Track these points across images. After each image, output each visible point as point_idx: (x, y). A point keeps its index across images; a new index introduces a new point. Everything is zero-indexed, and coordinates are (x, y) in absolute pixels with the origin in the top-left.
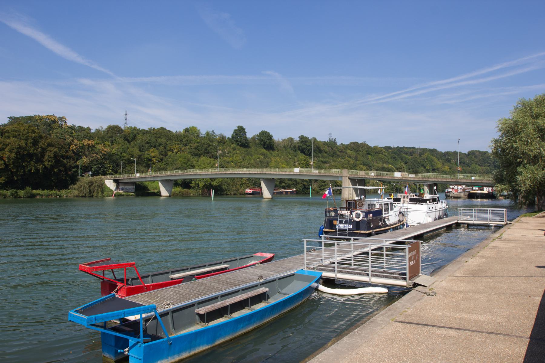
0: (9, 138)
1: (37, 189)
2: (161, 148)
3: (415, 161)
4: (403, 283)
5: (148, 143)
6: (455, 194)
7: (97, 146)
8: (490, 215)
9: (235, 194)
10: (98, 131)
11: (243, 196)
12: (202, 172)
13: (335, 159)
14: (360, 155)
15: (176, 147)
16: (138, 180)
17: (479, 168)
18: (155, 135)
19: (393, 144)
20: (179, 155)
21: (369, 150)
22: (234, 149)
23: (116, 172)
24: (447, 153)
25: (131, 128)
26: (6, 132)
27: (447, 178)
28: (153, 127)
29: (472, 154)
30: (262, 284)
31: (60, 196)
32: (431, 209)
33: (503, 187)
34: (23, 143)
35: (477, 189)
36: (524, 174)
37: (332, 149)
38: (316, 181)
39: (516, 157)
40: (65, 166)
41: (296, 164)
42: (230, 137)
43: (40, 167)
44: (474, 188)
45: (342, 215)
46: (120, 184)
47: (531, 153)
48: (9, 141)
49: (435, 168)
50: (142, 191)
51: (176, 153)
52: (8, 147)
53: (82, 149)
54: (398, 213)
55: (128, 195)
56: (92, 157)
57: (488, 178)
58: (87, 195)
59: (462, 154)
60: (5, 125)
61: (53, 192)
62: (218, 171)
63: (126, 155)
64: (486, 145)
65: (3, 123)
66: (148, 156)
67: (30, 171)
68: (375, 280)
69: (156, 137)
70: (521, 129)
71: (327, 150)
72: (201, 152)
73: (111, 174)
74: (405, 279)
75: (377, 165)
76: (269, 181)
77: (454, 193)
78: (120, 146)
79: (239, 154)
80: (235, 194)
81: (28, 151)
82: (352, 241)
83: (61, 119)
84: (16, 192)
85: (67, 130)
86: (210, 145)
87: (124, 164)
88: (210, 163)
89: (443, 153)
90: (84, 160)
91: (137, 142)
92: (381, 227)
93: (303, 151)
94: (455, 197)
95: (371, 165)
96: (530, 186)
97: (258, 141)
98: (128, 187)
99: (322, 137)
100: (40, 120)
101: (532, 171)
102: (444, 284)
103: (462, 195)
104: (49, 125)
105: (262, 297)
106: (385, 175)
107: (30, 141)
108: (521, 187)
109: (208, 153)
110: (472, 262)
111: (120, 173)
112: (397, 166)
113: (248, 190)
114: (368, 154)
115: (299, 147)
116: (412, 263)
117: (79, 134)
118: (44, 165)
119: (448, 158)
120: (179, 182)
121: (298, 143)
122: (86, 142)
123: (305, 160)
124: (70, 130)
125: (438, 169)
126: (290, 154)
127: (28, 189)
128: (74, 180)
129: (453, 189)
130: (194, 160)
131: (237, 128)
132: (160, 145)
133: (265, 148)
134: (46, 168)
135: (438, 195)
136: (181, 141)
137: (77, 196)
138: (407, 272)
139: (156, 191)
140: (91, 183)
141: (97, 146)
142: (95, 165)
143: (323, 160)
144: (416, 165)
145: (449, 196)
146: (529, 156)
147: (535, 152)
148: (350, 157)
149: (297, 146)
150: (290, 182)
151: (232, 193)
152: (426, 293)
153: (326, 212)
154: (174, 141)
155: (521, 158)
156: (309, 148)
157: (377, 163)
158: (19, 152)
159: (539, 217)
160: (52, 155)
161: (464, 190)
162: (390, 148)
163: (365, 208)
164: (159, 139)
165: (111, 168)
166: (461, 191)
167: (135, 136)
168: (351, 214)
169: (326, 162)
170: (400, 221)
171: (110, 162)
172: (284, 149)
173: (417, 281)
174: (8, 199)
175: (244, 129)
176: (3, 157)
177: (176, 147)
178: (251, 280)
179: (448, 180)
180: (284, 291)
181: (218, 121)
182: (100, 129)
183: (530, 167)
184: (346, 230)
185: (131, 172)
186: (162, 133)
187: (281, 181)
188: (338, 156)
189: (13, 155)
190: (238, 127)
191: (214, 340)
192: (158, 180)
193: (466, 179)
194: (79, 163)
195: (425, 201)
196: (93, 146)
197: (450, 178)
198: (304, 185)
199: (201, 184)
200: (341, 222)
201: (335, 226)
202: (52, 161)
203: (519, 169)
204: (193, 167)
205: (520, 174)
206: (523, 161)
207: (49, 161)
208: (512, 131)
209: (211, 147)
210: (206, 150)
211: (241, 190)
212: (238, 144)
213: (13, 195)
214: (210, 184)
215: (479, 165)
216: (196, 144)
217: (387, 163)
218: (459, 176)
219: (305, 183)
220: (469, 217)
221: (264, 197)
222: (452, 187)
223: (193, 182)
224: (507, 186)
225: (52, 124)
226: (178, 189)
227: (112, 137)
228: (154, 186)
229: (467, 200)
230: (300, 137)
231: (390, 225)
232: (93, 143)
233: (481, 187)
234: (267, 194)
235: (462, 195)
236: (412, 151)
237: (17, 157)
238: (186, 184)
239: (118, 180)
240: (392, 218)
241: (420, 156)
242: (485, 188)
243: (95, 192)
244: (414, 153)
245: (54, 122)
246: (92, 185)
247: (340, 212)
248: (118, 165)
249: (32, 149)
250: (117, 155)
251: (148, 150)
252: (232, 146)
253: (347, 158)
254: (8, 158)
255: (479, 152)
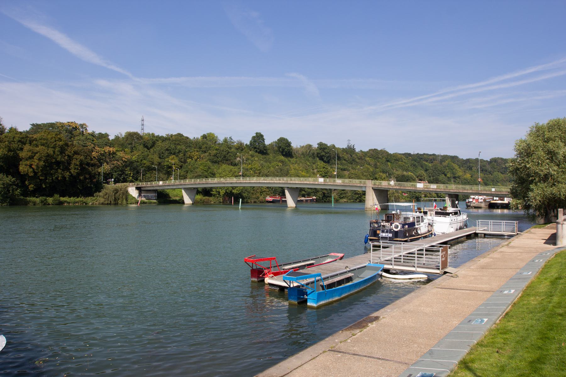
0: (37, 146)
1: (64, 197)
2: (181, 155)
3: (435, 168)
4: (438, 271)
5: (167, 150)
6: (476, 204)
7: (118, 153)
8: (503, 227)
9: (255, 202)
10: (117, 138)
11: (263, 204)
12: (222, 181)
13: (354, 166)
14: (379, 162)
15: (195, 154)
16: (161, 188)
17: (501, 176)
18: (174, 142)
19: (413, 151)
20: (200, 162)
21: (389, 157)
22: (252, 156)
23: (137, 180)
24: (468, 161)
25: (149, 134)
26: (34, 140)
27: (468, 189)
28: (171, 133)
29: (494, 161)
30: (349, 271)
31: (86, 204)
32: (453, 221)
33: (518, 201)
34: (51, 151)
35: (497, 198)
36: (536, 191)
37: (351, 156)
38: (335, 190)
39: (529, 175)
40: (90, 173)
41: (315, 171)
42: (248, 143)
43: (67, 174)
44: (495, 198)
45: (384, 226)
46: (142, 192)
47: (542, 173)
48: (38, 149)
49: (456, 175)
50: (163, 198)
51: (196, 160)
52: (37, 155)
53: (103, 156)
54: (427, 225)
55: (151, 203)
56: (113, 164)
57: (505, 189)
58: (112, 202)
59: (484, 161)
60: (27, 132)
61: (79, 199)
62: (241, 180)
63: (147, 163)
64: (508, 153)
65: (25, 130)
66: (168, 163)
67: (57, 178)
68: (419, 270)
69: (175, 144)
70: (533, 151)
71: (346, 157)
72: (220, 159)
73: (131, 181)
74: (439, 269)
75: (397, 173)
76: (293, 190)
77: (474, 204)
78: (140, 153)
79: (258, 161)
80: (255, 202)
81: (56, 159)
82: (402, 245)
83: (82, 126)
84: (46, 200)
85: (88, 137)
86: (229, 152)
87: (144, 171)
88: (231, 171)
89: (464, 160)
90: (105, 168)
91: (157, 149)
92: (414, 236)
93: (321, 158)
94: (475, 207)
95: (390, 172)
96: (540, 201)
97: (276, 148)
98: (150, 195)
99: (341, 144)
100: (62, 127)
101: (542, 188)
102: (463, 272)
103: (483, 205)
104: (71, 132)
105: (349, 279)
106: (408, 186)
107: (57, 149)
108: (532, 202)
109: (227, 160)
110: (483, 261)
111: (140, 181)
112: (418, 174)
113: (269, 198)
114: (388, 161)
115: (318, 154)
116: (443, 259)
117: (100, 141)
118: (70, 172)
119: (468, 164)
120: (200, 190)
121: (316, 150)
122: (107, 149)
123: (324, 168)
124: (91, 137)
125: (459, 177)
126: (308, 161)
127: (57, 196)
128: (98, 187)
129: (474, 198)
130: (214, 168)
131: (255, 135)
132: (180, 152)
133: (284, 155)
134: (72, 175)
135: (459, 209)
136: (200, 148)
137: (102, 204)
138: (440, 265)
139: (177, 199)
140: (116, 191)
141: (118, 153)
142: (116, 172)
143: (341, 167)
144: (437, 173)
145: (470, 206)
146: (540, 175)
147: (545, 172)
148: (369, 164)
149: (316, 153)
150: (310, 190)
151: (253, 201)
152: (452, 276)
153: (371, 223)
154: (193, 148)
155: (533, 176)
156: (328, 155)
157: (397, 170)
158: (47, 160)
159: (548, 228)
160: (78, 163)
161: (485, 200)
162: (409, 155)
163: (402, 220)
164: (177, 144)
165: (132, 175)
166: (482, 201)
167: (154, 144)
168: (391, 225)
169: (344, 170)
170: (429, 231)
171: (130, 169)
172: (302, 156)
173: (446, 270)
174: (37, 206)
175: (262, 136)
176: (32, 164)
177: (195, 154)
178: (340, 269)
179: (469, 192)
180: (361, 276)
181: (236, 127)
182: (119, 135)
183: (542, 185)
184: (387, 238)
185: (151, 179)
186: (179, 139)
187: (301, 189)
188: (357, 163)
189: (42, 163)
190: (257, 133)
191: (341, 294)
192: (182, 189)
193: (486, 191)
194: (101, 170)
195: (448, 214)
196: (114, 153)
197: (471, 189)
198: (324, 193)
199: (222, 192)
200: (383, 232)
201: (378, 234)
202: (78, 169)
203: (532, 186)
204: (213, 175)
205: (532, 190)
206: (535, 179)
207: (75, 169)
208: (526, 152)
209: (229, 154)
210: (225, 157)
211: (261, 198)
212: (256, 151)
213: (42, 202)
214: (231, 192)
215: (501, 173)
216: (215, 152)
217: (407, 170)
218: (480, 188)
219: (324, 191)
220: (486, 228)
221: (289, 206)
222: (472, 197)
223: (214, 190)
224: (521, 201)
225: (73, 131)
226: (199, 197)
227: (131, 144)
228: (175, 193)
229: (488, 210)
230: (318, 144)
231: (421, 234)
232: (115, 150)
233: (502, 197)
234: (291, 202)
235: (483, 205)
236: (432, 158)
237: (45, 165)
238: (207, 192)
239: (140, 188)
240: (423, 228)
241: (441, 163)
242: (505, 198)
243: (119, 200)
244: (434, 160)
245: (76, 128)
246: (117, 192)
247: (382, 224)
248: (138, 172)
249: (60, 156)
250: (138, 162)
251: (168, 157)
252: (250, 152)
253: (367, 166)
254: (37, 166)
255: (502, 159)
